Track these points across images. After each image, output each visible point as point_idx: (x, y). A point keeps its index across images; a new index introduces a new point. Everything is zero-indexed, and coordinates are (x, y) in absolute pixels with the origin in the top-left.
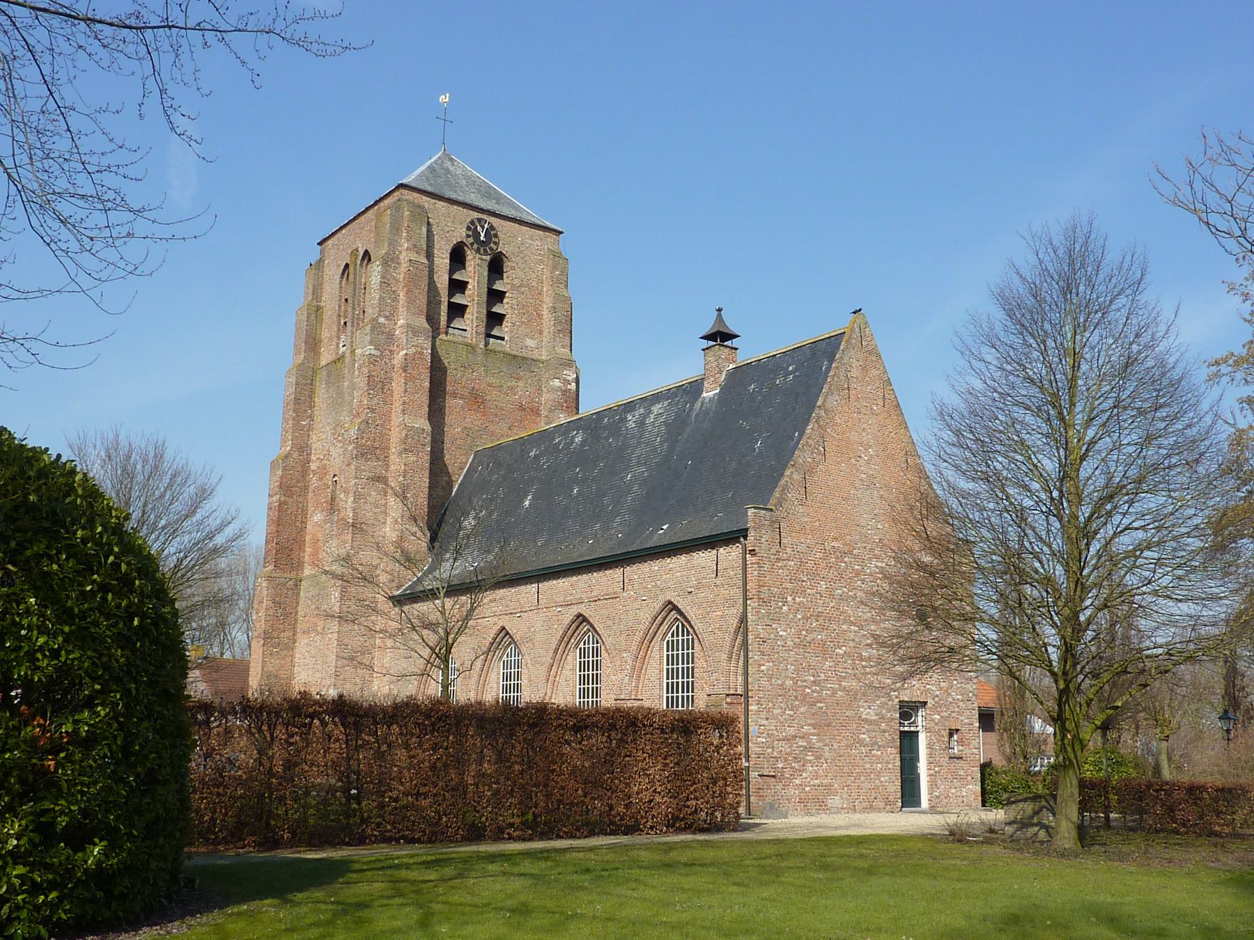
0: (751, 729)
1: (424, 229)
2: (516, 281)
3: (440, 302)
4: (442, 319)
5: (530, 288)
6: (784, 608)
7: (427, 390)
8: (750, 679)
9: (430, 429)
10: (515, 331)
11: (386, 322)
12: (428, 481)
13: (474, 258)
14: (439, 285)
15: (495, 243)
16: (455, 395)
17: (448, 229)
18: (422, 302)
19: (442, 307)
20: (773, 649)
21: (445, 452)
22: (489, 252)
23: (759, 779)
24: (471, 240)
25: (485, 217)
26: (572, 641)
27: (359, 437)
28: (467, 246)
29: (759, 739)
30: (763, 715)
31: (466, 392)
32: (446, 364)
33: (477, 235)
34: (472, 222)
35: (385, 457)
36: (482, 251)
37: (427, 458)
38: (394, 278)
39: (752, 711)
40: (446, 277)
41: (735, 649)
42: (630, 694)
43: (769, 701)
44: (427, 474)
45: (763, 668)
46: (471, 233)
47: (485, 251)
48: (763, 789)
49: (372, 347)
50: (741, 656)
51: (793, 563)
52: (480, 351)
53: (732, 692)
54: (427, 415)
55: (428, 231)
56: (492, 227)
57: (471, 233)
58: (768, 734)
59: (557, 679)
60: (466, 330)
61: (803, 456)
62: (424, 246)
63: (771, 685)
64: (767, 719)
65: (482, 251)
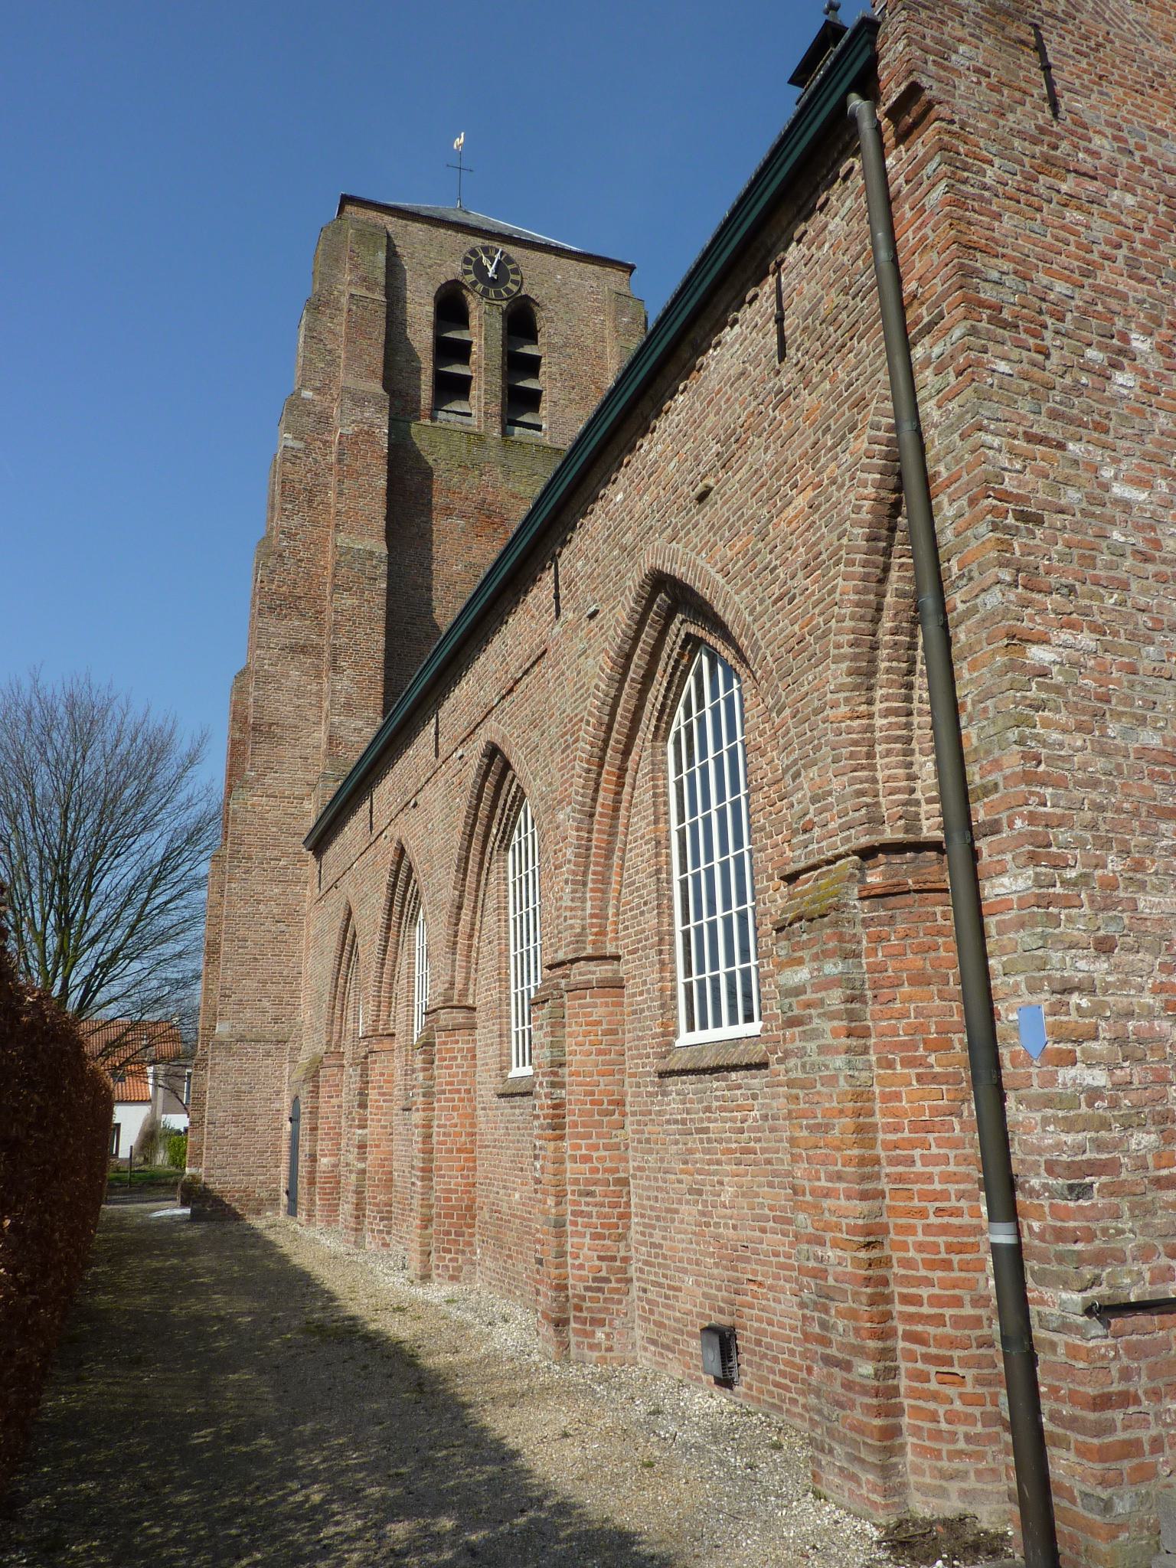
0: (1008, 1014)
1: (382, 256)
2: (556, 339)
3: (419, 370)
4: (423, 395)
5: (582, 348)
6: (1120, 378)
7: (383, 492)
8: (971, 735)
9: (385, 552)
10: (558, 415)
11: (317, 398)
12: (382, 639)
13: (479, 304)
14: (415, 344)
15: (515, 282)
16: (448, 511)
17: (431, 262)
18: (377, 356)
19: (423, 377)
20: (1091, 562)
21: (434, 603)
22: (505, 295)
23: (1097, 1337)
24: (472, 277)
25: (495, 244)
26: (494, 831)
27: (265, 579)
28: (466, 287)
29: (1066, 1074)
30: (1077, 923)
31: (469, 507)
32: (431, 462)
33: (481, 270)
34: (473, 252)
35: (317, 612)
36: (492, 294)
37: (381, 600)
38: (331, 331)
39: (1004, 905)
40: (429, 333)
41: (887, 624)
42: (579, 939)
43: (1105, 844)
44: (380, 627)
45: (1039, 654)
46: (471, 268)
47: (498, 294)
48: (1126, 1399)
49: (289, 436)
50: (921, 692)
51: (1130, 200)
52: (493, 443)
53: (890, 833)
54: (383, 534)
55: (388, 259)
56: (509, 260)
57: (471, 268)
58: (1119, 1040)
59: (475, 941)
60: (469, 415)
61: (1148, 1298)
62: (382, 280)
63: (1103, 752)
64: (1104, 947)
65: (492, 294)
